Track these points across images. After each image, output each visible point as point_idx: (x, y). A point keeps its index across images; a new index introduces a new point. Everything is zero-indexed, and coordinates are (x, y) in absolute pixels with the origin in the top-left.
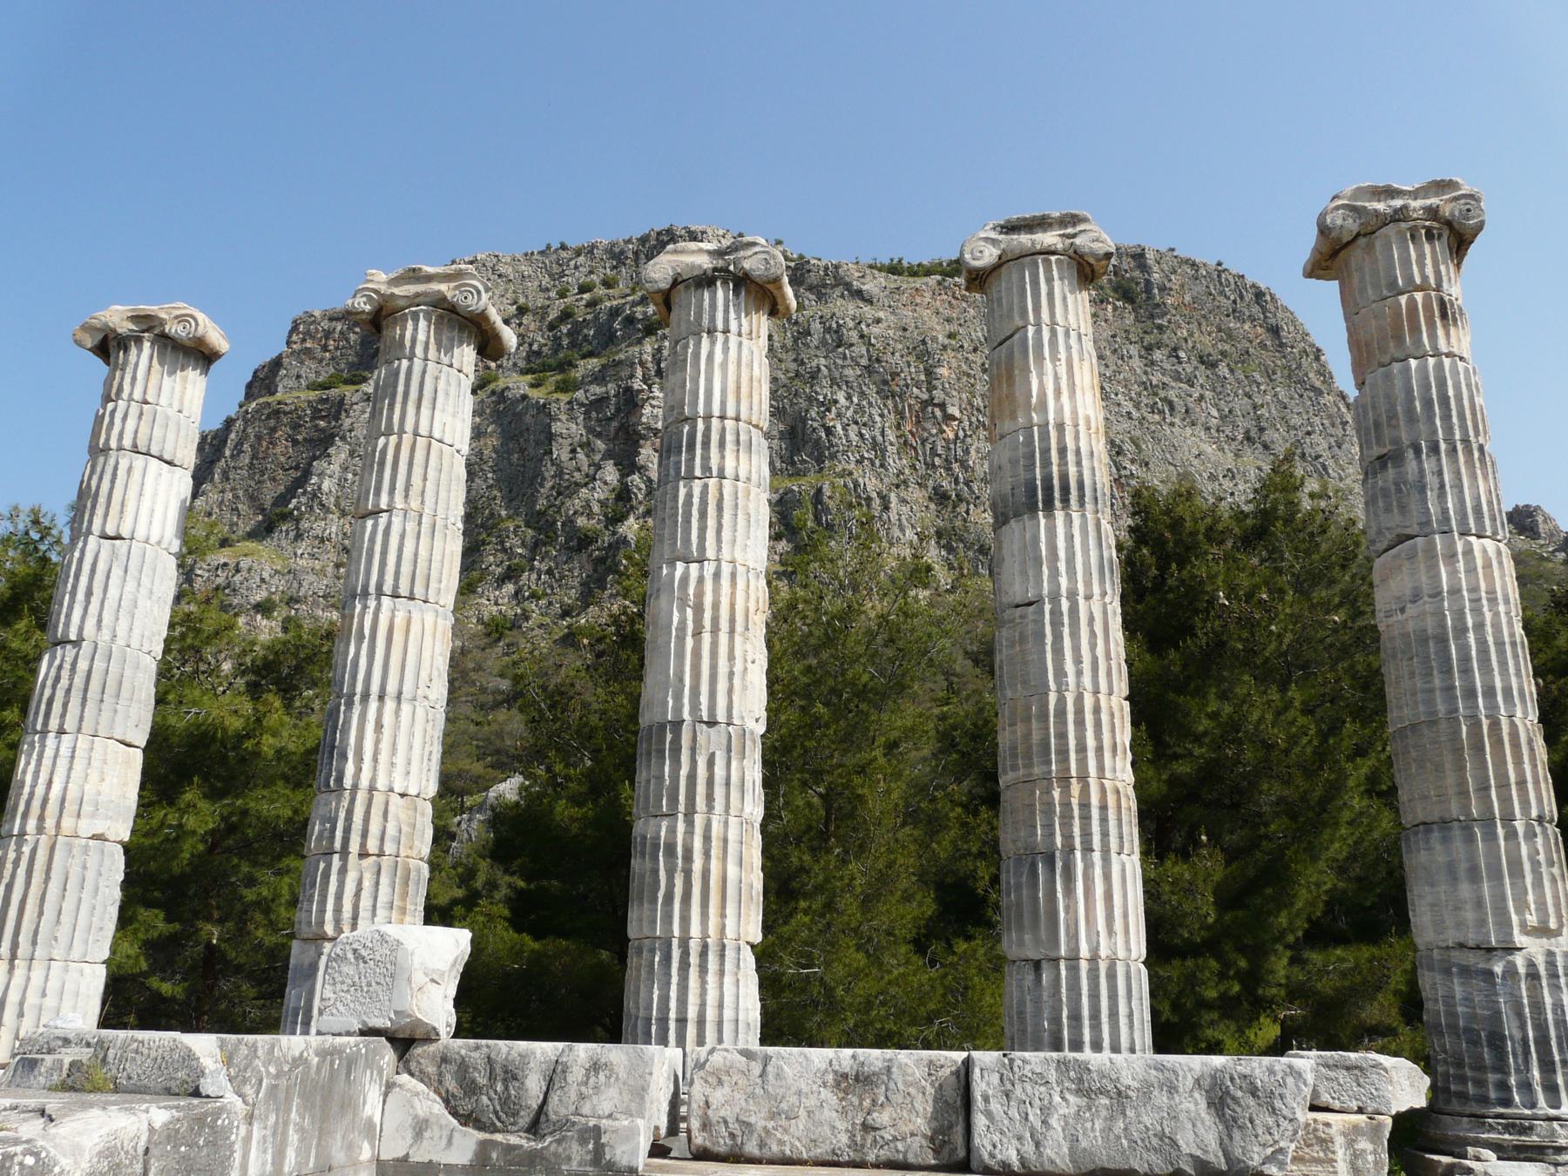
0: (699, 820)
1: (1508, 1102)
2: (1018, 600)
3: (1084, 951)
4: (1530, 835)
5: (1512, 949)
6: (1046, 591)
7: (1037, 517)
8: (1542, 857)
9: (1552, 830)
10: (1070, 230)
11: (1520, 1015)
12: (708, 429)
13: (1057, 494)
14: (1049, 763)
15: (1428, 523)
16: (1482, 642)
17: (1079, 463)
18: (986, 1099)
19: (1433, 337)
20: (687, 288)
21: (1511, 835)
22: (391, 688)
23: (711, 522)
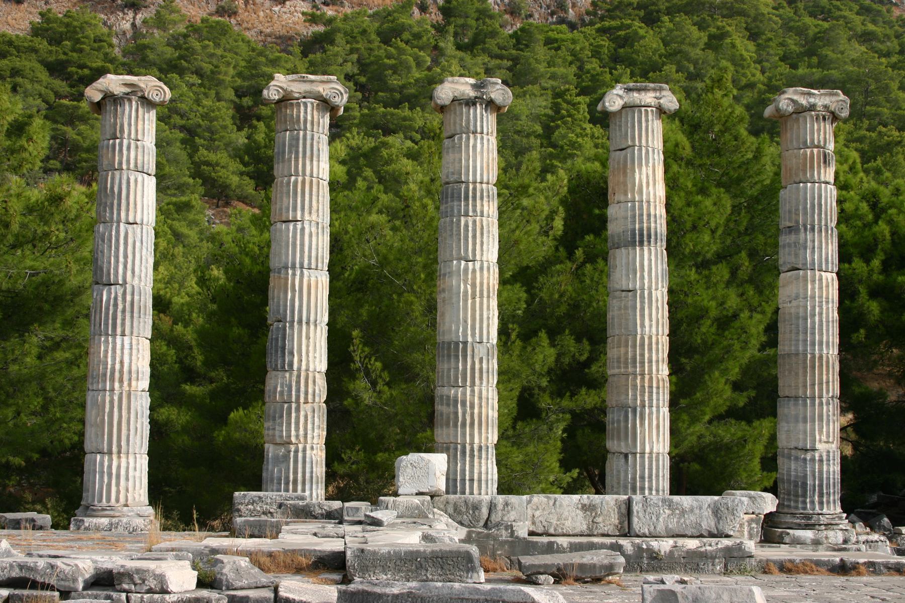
0: (476, 389)
1: (805, 508)
2: (624, 288)
3: (647, 450)
4: (828, 404)
5: (814, 450)
6: (638, 287)
8: (831, 413)
9: (837, 401)
10: (658, 94)
11: (814, 476)
12: (475, 189)
13: (645, 239)
14: (636, 367)
15: (806, 264)
16: (821, 321)
17: (656, 222)
18: (638, 512)
19: (819, 173)
20: (460, 104)
21: (821, 404)
22: (312, 319)
23: (478, 241)
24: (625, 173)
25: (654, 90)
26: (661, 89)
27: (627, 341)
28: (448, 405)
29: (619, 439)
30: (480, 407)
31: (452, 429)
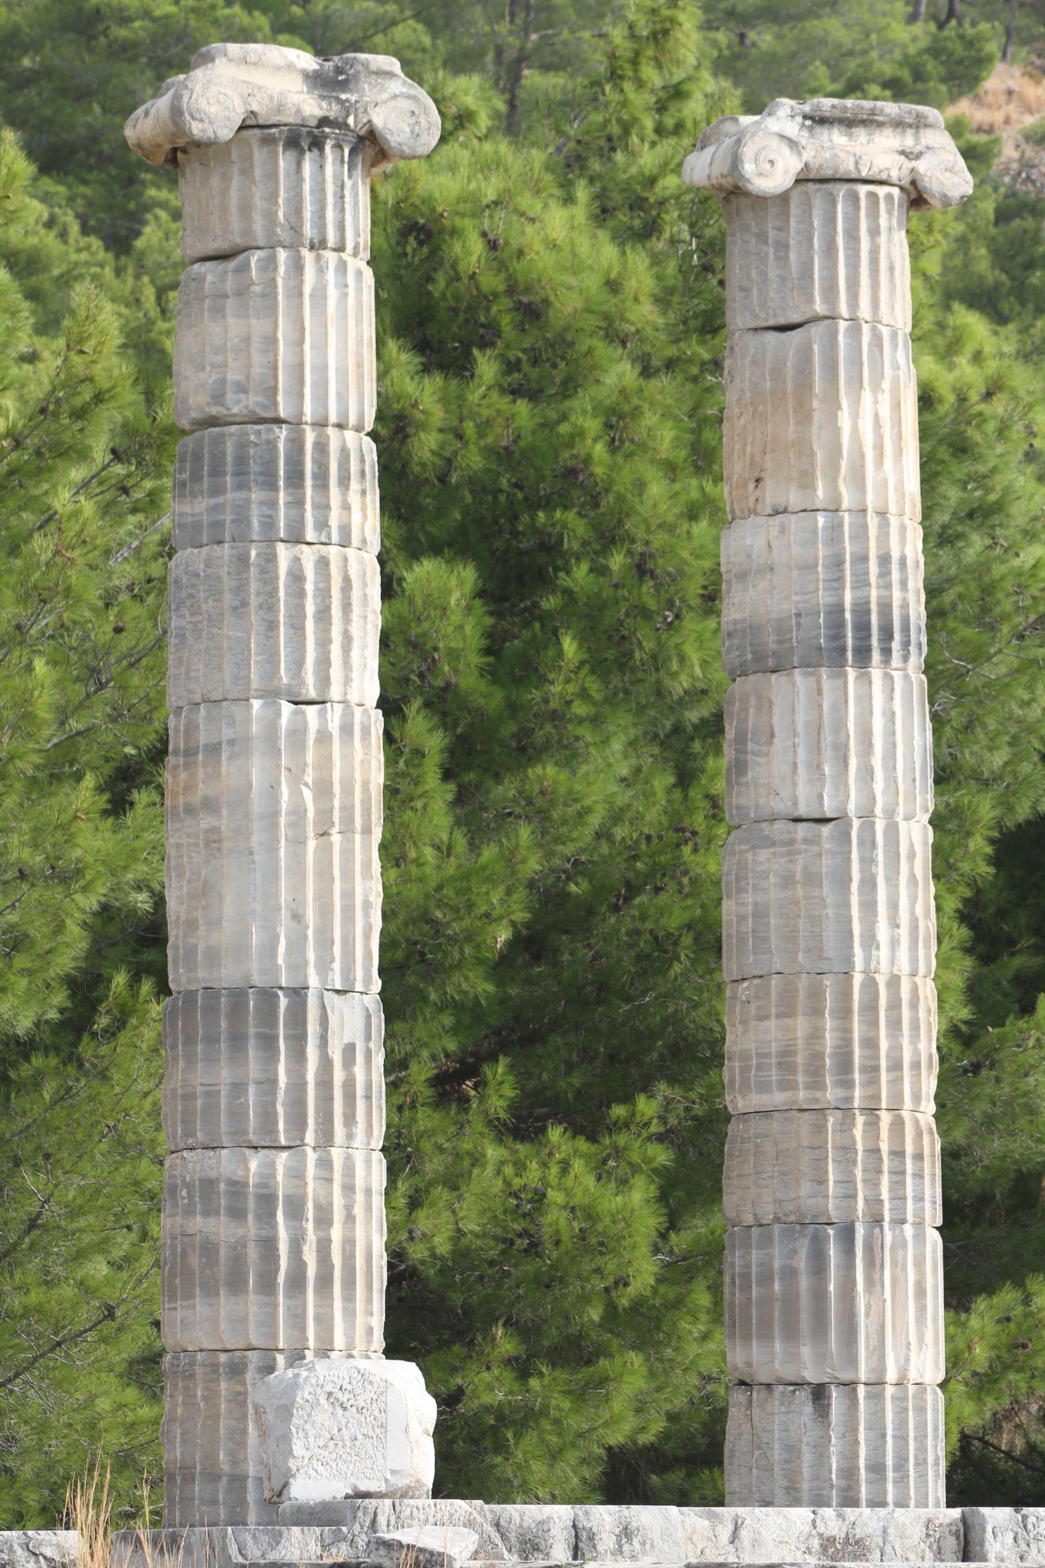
0: (337, 1154)
2: (803, 811)
7: (845, 675)
12: (322, 447)
13: (875, 642)
14: (849, 1085)
24: (804, 415)
25: (899, 124)
26: (919, 124)
27: (816, 995)
28: (237, 1213)
29: (791, 1335)
30: (350, 1219)
31: (253, 1303)
